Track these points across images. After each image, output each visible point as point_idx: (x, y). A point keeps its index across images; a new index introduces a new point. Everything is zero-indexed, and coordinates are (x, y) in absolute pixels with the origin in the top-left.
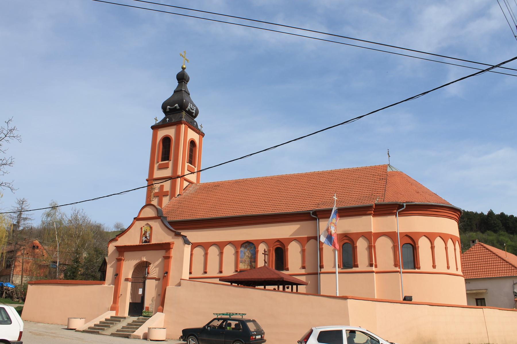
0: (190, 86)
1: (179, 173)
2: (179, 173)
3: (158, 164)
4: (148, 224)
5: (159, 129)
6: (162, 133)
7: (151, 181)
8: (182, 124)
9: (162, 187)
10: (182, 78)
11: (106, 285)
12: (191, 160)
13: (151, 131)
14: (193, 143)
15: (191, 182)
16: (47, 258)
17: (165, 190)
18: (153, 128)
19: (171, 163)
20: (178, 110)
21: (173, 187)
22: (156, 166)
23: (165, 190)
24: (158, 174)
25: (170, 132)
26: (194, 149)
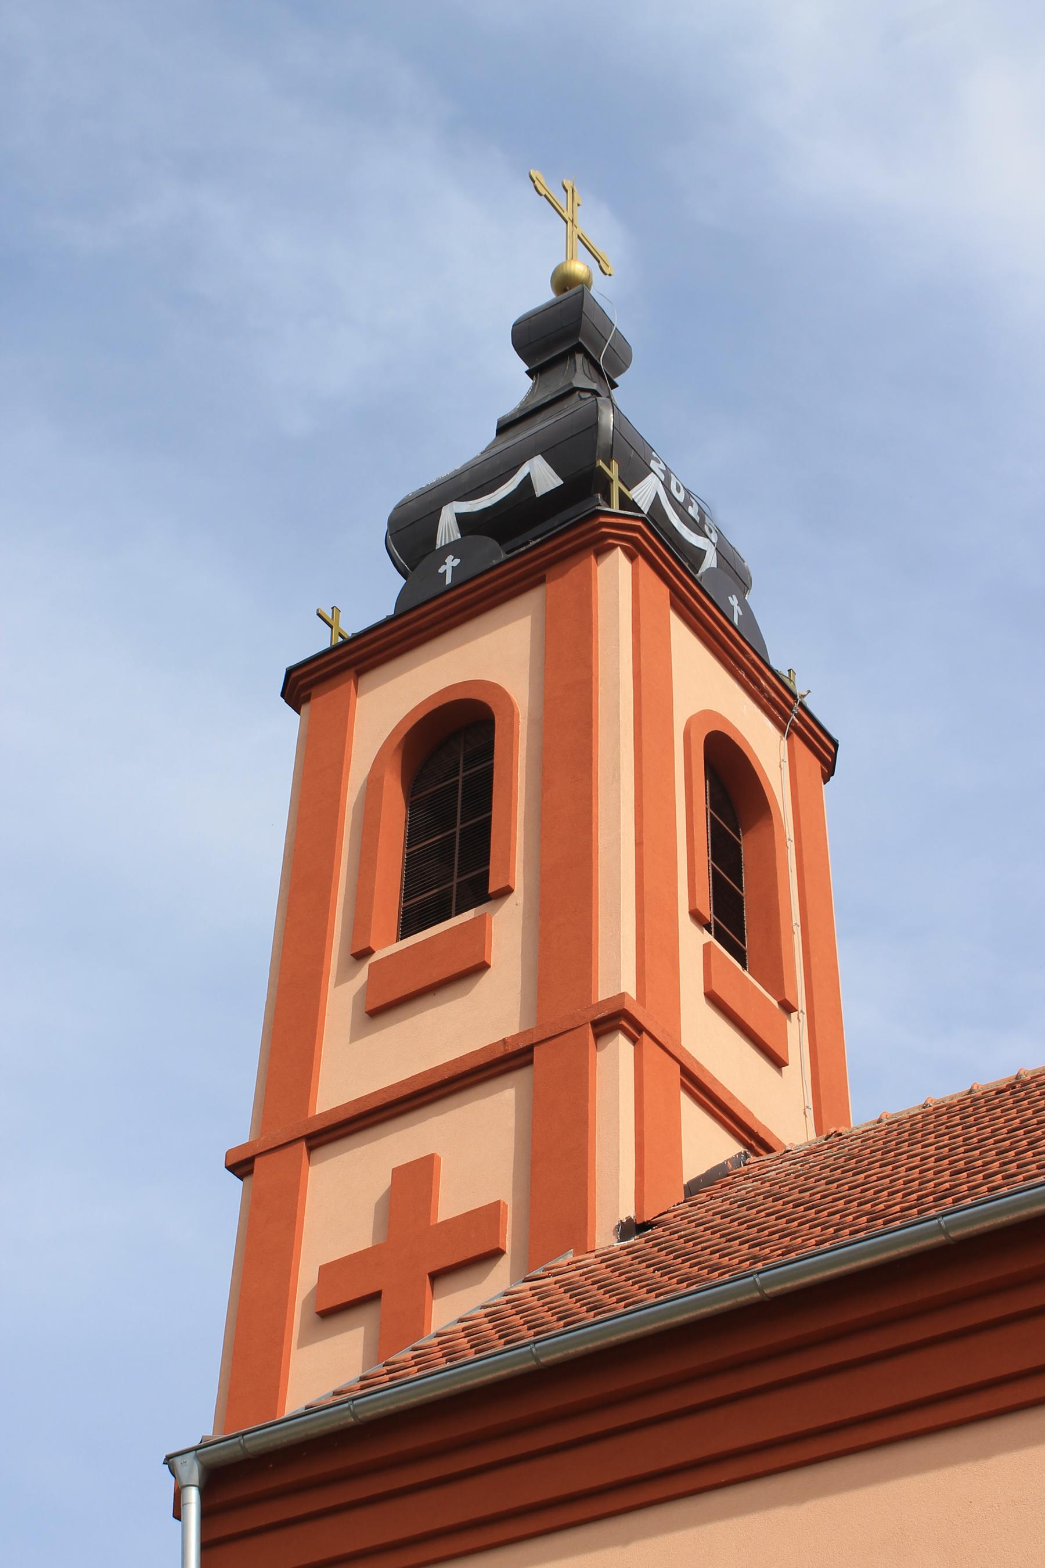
0: (635, 401)
1: (617, 976)
2: (617, 976)
3: (363, 975)
4: (499, 1253)
5: (366, 680)
6: (385, 707)
7: (272, 1159)
8: (602, 550)
9: (416, 1179)
10: (562, 338)
11: (741, 843)
12: (732, 915)
13: (289, 722)
14: (726, 767)
15: (753, 1139)
16: (331, 1313)
17: (451, 1202)
18: (301, 685)
19: (507, 928)
20: (547, 506)
21: (557, 1154)
22: (341, 996)
23: (451, 1202)
24: (352, 1067)
25: (496, 655)
26: (748, 845)
